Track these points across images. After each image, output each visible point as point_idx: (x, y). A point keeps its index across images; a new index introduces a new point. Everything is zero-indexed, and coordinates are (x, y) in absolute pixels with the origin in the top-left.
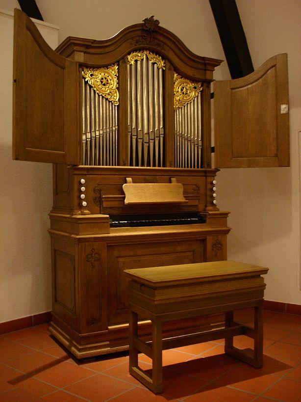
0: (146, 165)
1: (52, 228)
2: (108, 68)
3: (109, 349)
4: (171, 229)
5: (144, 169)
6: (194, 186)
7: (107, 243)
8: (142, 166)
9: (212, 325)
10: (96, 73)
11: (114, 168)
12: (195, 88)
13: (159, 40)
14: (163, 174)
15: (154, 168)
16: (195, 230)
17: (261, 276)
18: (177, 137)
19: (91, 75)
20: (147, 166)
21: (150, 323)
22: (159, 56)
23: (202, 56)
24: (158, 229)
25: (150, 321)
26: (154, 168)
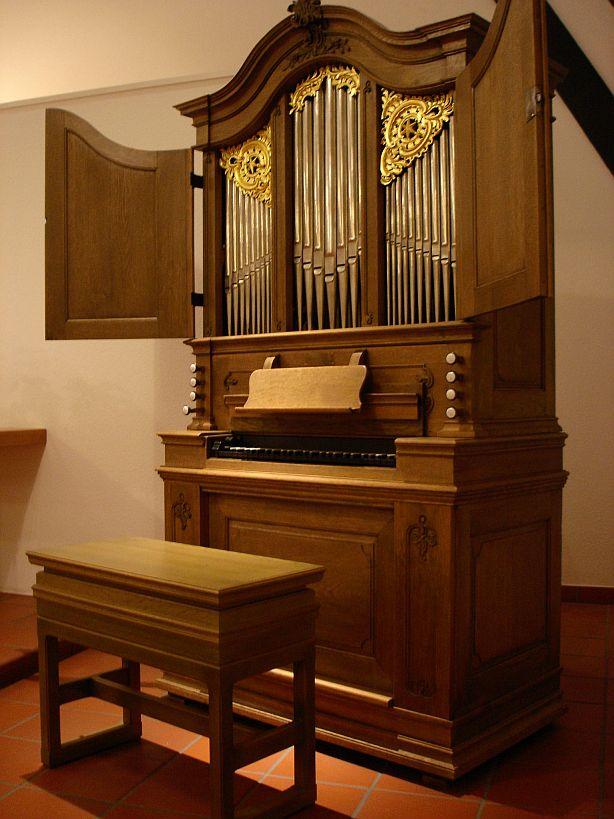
0: (310, 326)
1: (169, 459)
2: (258, 137)
3: (198, 691)
4: (340, 476)
5: (298, 336)
6: (420, 371)
7: (201, 488)
8: (324, 328)
9: (400, 737)
10: (238, 155)
11: (242, 340)
12: (436, 111)
13: (363, 29)
14: (244, 348)
15: (315, 332)
16: (370, 483)
17: (308, 586)
18: (390, 246)
19: (233, 161)
20: (335, 328)
21: (289, 678)
22: (345, 69)
23: (412, 28)
24: (282, 471)
25: (291, 675)
26: (315, 332)
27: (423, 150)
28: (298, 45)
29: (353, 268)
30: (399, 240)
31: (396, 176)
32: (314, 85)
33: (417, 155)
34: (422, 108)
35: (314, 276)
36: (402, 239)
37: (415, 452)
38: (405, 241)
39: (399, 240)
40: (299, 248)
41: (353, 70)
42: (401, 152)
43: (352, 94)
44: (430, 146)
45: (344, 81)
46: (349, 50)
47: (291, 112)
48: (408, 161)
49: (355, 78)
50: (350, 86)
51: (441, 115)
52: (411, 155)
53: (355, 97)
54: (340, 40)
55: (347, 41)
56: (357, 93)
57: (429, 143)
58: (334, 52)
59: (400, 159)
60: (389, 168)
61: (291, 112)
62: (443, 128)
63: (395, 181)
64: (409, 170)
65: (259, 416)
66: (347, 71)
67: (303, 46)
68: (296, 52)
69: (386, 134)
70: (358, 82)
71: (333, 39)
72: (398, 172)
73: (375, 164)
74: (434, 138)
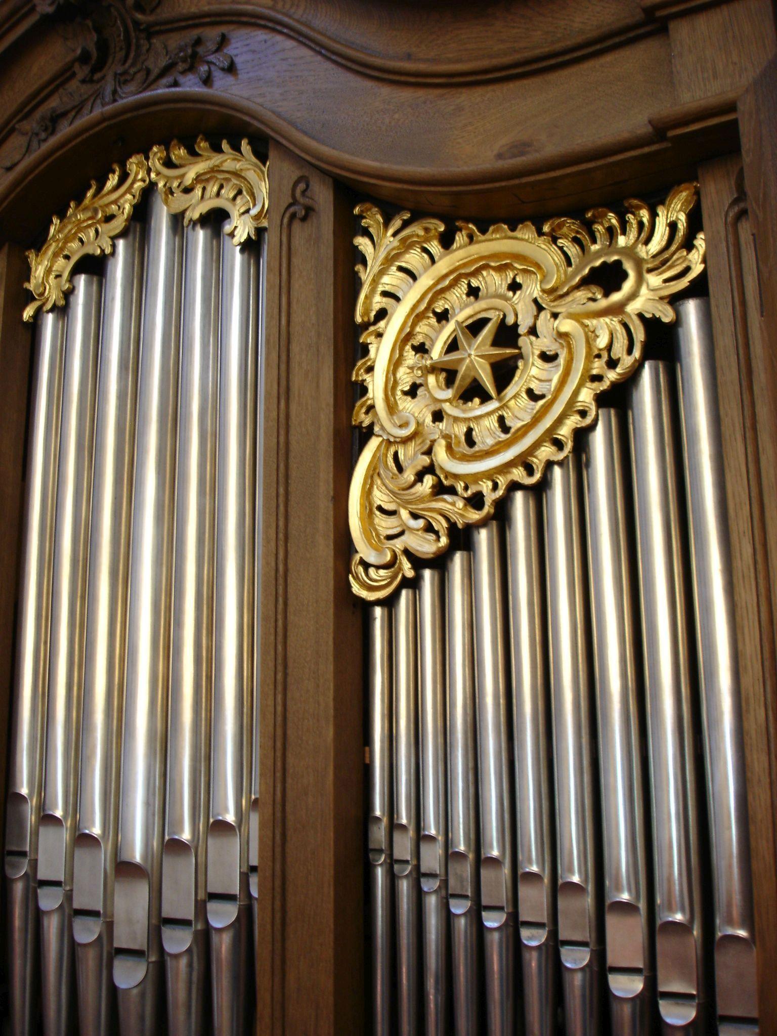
27: (547, 452)
28: (63, 77)
29: (223, 945)
30: (432, 858)
31: (418, 563)
32: (109, 218)
33: (518, 474)
34: (534, 266)
35: (73, 949)
36: (451, 855)
37: (280, 623)
38: (467, 869)
39: (432, 858)
40: (379, 834)
41: (245, 146)
42: (441, 455)
43: (241, 235)
44: (582, 436)
45: (213, 189)
46: (231, 69)
47: (28, 313)
48: (476, 501)
49: (251, 175)
50: (235, 211)
51: (633, 296)
52: (489, 475)
53: (251, 247)
54: (198, 42)
55: (224, 41)
56: (260, 231)
57: (573, 421)
58: (176, 84)
59: (440, 489)
60: (386, 525)
61: (28, 313)
62: (648, 354)
63: (414, 584)
64: (483, 537)
65: (367, 761)
66: (227, 160)
67: (74, 84)
68: (54, 103)
69: (376, 386)
70: (263, 189)
71: (175, 41)
72: (427, 547)
73: (325, 507)
74: (602, 400)
